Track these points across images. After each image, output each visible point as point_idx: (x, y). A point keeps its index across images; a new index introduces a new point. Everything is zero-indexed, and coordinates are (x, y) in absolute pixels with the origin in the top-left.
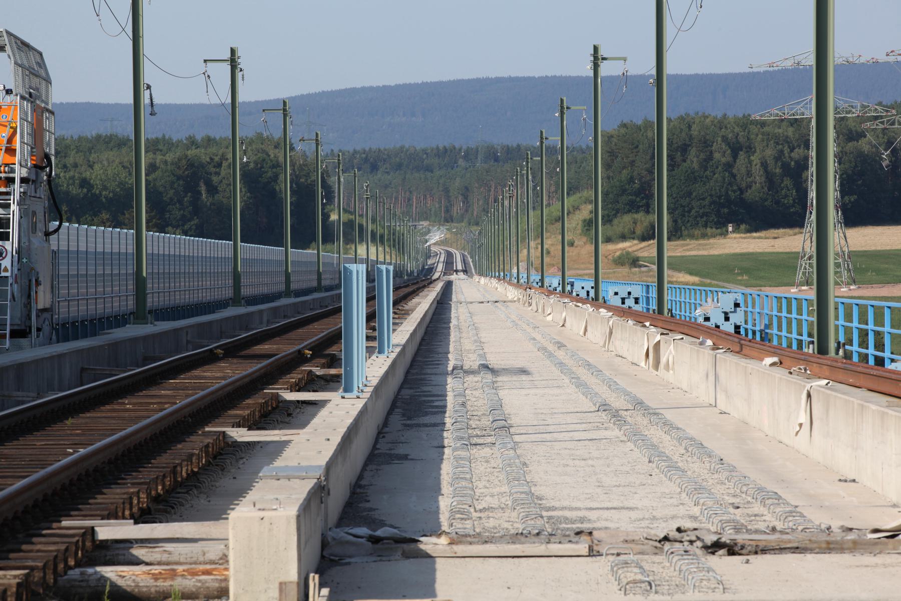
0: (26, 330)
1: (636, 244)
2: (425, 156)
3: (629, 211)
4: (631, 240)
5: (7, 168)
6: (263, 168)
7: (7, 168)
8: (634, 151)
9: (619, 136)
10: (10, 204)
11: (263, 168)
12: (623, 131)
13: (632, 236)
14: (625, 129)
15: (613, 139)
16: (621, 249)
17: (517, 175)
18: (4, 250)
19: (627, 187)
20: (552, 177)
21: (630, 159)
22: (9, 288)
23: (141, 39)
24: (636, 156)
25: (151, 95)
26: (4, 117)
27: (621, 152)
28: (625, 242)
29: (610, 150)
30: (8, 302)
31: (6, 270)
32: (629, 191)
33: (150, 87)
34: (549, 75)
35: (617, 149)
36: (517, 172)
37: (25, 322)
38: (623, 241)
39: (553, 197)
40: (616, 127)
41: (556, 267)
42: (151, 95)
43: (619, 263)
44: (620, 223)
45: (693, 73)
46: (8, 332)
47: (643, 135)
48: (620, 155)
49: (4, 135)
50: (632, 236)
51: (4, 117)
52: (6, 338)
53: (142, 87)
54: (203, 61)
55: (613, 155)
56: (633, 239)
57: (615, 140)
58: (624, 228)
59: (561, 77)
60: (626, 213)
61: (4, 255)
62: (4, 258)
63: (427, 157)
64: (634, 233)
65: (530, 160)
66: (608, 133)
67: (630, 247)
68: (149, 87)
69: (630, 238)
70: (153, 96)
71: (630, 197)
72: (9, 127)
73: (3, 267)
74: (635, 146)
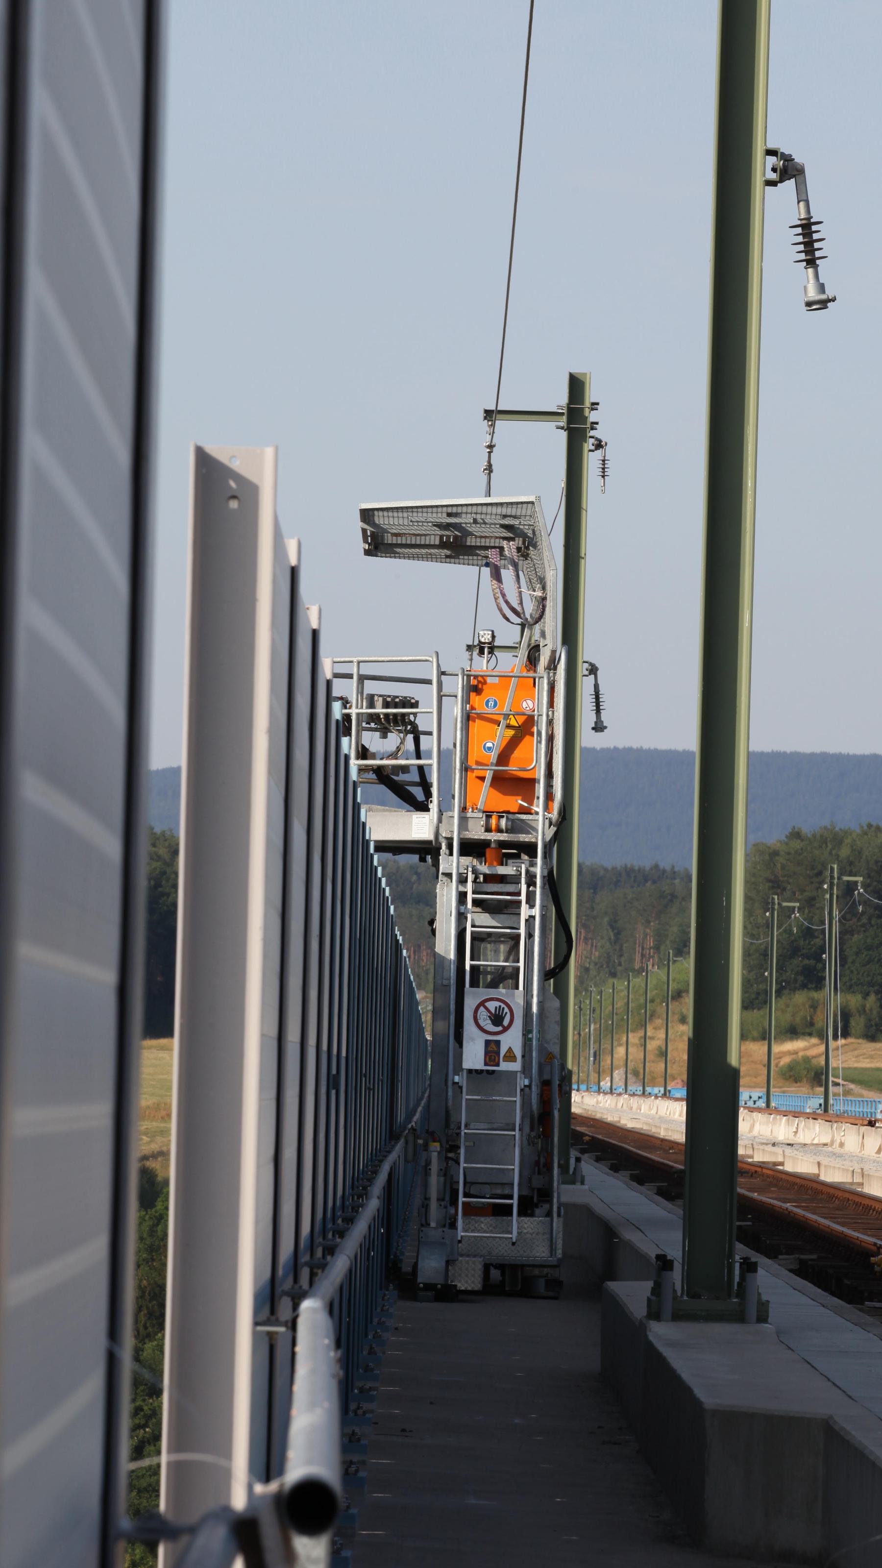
0: (532, 1197)
1: (814, 1045)
2: (414, 878)
3: (804, 986)
4: (807, 1038)
5: (503, 822)
6: (160, 886)
7: (503, 822)
8: (816, 880)
9: (789, 854)
10: (520, 902)
11: (160, 886)
12: (796, 844)
13: (808, 1030)
14: (799, 841)
15: (777, 858)
16: (789, 1053)
17: (773, 909)
18: (506, 1010)
19: (802, 943)
20: (649, 922)
21: (806, 894)
22: (518, 1099)
23: (582, 561)
24: (817, 889)
25: (596, 686)
26: (491, 703)
27: (791, 881)
28: (797, 1039)
29: (772, 878)
30: (517, 1133)
31: (510, 1056)
32: (804, 951)
33: (597, 669)
34: (621, 746)
35: (785, 876)
36: (773, 903)
37: (530, 1180)
38: (791, 1039)
39: (650, 957)
40: (783, 838)
41: (679, 1081)
42: (596, 686)
43: (790, 1077)
44: (788, 1006)
45: (867, 752)
46: (515, 1202)
47: (830, 853)
48: (789, 887)
49: (489, 745)
50: (808, 1030)
51: (491, 703)
52: (511, 1214)
53: (582, 669)
54: (465, 648)
55: (779, 887)
56: (810, 1035)
57: (781, 860)
58: (794, 1015)
59: (640, 751)
60: (799, 990)
61: (506, 1022)
62: (506, 1029)
63: (419, 879)
64: (812, 1024)
65: (836, 881)
66: (769, 848)
67: (805, 1049)
68: (593, 670)
69: (804, 1034)
70: (602, 690)
71: (806, 962)
72: (503, 723)
73: (503, 1050)
74: (816, 871)
